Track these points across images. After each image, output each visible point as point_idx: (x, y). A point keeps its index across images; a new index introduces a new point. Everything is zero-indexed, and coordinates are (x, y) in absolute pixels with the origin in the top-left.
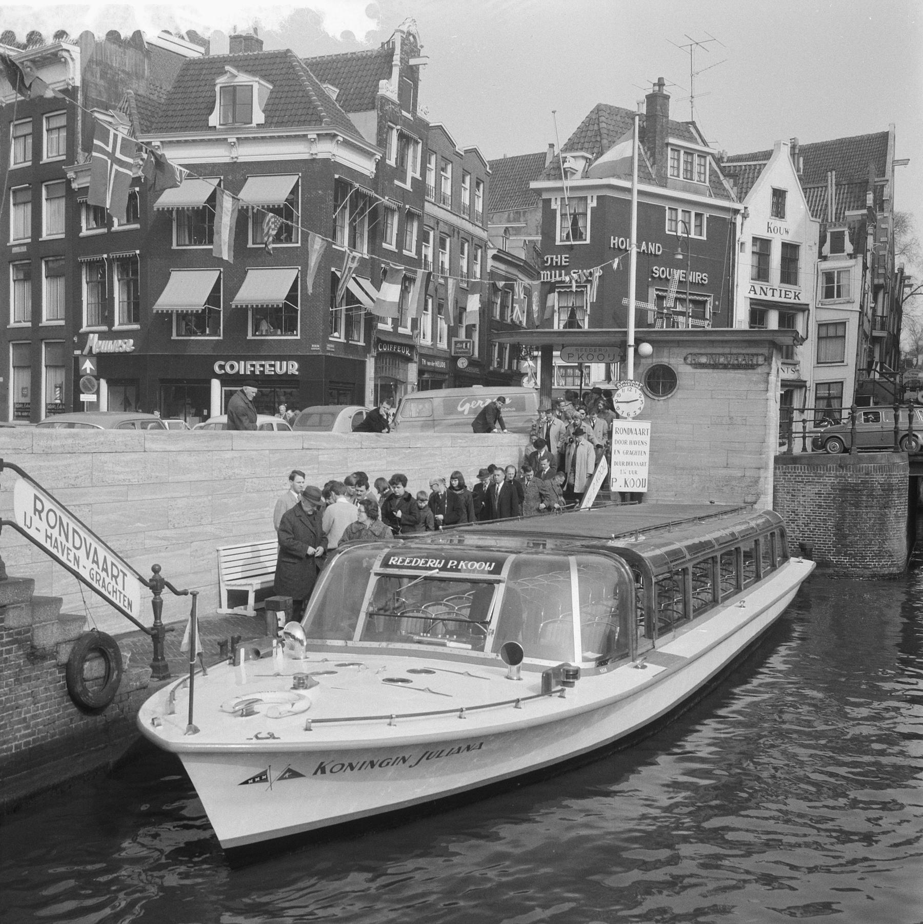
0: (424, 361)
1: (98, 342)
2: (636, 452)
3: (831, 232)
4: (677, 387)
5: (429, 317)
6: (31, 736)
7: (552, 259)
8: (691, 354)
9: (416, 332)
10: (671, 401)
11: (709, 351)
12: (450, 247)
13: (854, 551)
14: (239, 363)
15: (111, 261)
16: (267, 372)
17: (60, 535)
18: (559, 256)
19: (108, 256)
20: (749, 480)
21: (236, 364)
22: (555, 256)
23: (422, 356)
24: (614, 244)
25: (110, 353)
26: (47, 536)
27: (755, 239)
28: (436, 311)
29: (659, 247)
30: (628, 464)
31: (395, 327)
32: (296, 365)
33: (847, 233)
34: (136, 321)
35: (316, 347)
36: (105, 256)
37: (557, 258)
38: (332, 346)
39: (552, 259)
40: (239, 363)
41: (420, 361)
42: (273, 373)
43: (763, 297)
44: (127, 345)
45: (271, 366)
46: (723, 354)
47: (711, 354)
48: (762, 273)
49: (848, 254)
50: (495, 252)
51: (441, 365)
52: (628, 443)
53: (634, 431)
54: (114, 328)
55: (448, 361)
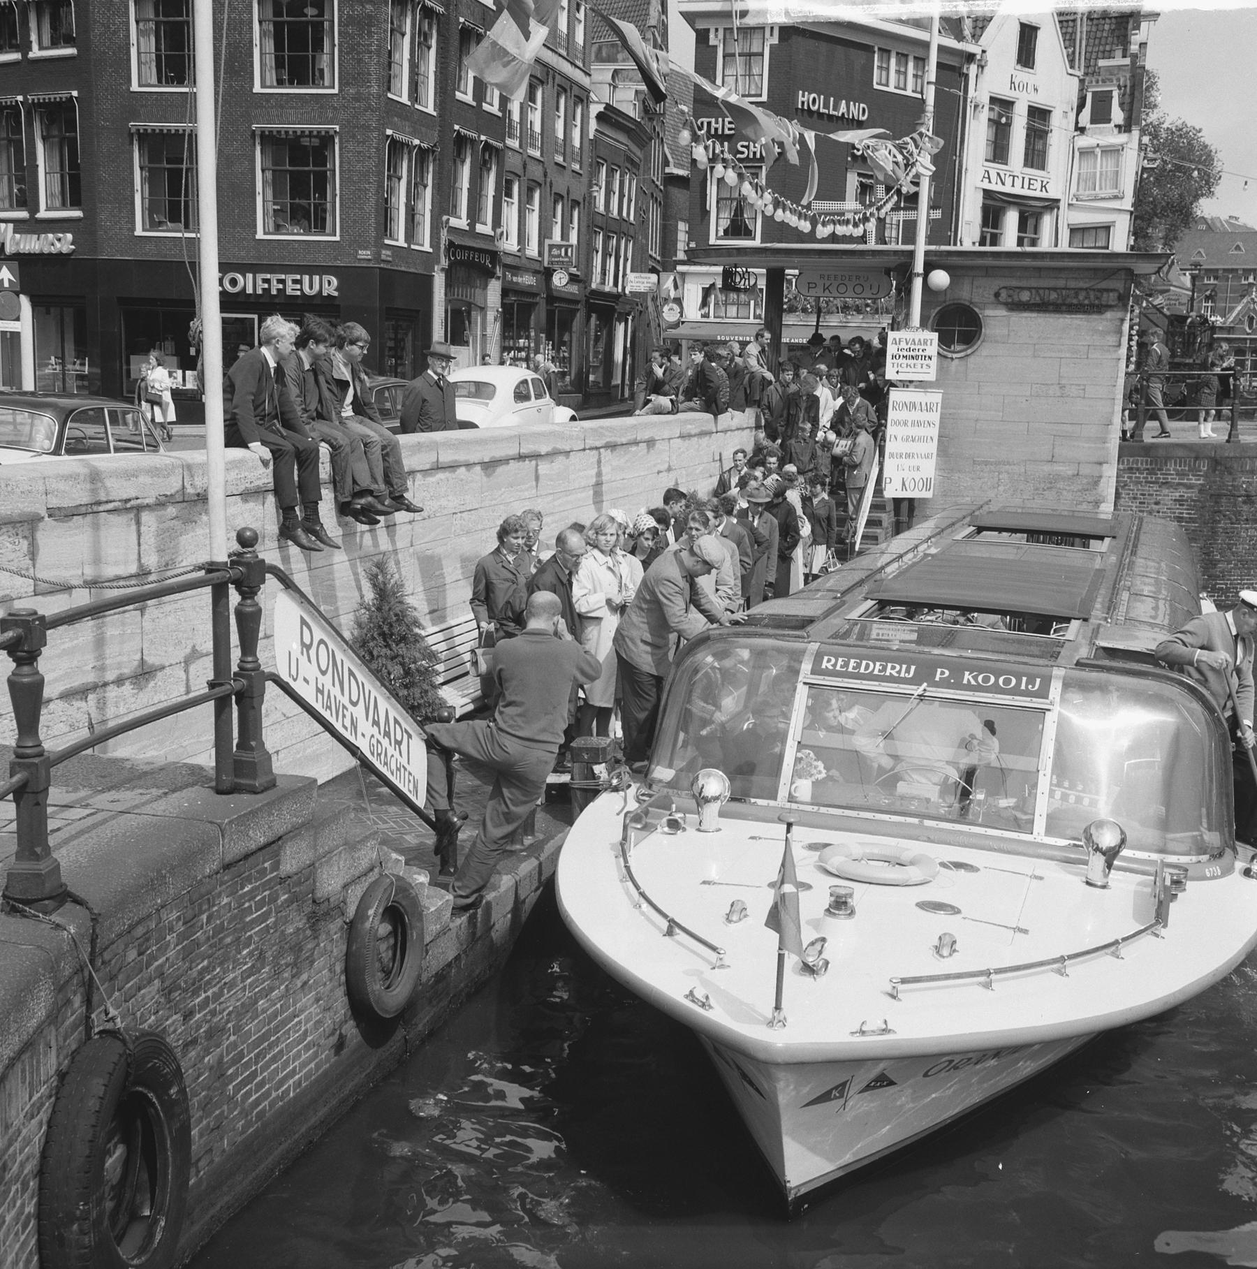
0: (509, 275)
1: (13, 238)
2: (919, 439)
3: (1093, 92)
4: (982, 338)
5: (515, 208)
6: (311, 1062)
7: (709, 124)
8: (1004, 288)
9: (499, 231)
10: (971, 359)
11: (1033, 283)
12: (543, 98)
13: (1226, 584)
14: (244, 277)
15: (31, 108)
16: (289, 292)
17: (334, 685)
18: (720, 120)
19: (25, 98)
20: (1085, 481)
21: (239, 277)
22: (713, 120)
23: (507, 267)
24: (803, 103)
25: (35, 254)
26: (318, 690)
27: (993, 100)
28: (524, 198)
29: (864, 109)
30: (908, 456)
31: (472, 225)
32: (335, 281)
33: (1116, 94)
34: (76, 203)
35: (364, 254)
36: (20, 98)
37: (717, 122)
38: (389, 253)
39: (709, 124)
40: (244, 277)
41: (504, 275)
42: (298, 293)
43: (999, 188)
44: (64, 243)
45: (295, 282)
46: (1055, 289)
47: (1037, 289)
48: (999, 152)
49: (1116, 126)
50: (601, 108)
51: (527, 280)
52: (909, 424)
53: (918, 407)
54: (38, 216)
55: (539, 276)
